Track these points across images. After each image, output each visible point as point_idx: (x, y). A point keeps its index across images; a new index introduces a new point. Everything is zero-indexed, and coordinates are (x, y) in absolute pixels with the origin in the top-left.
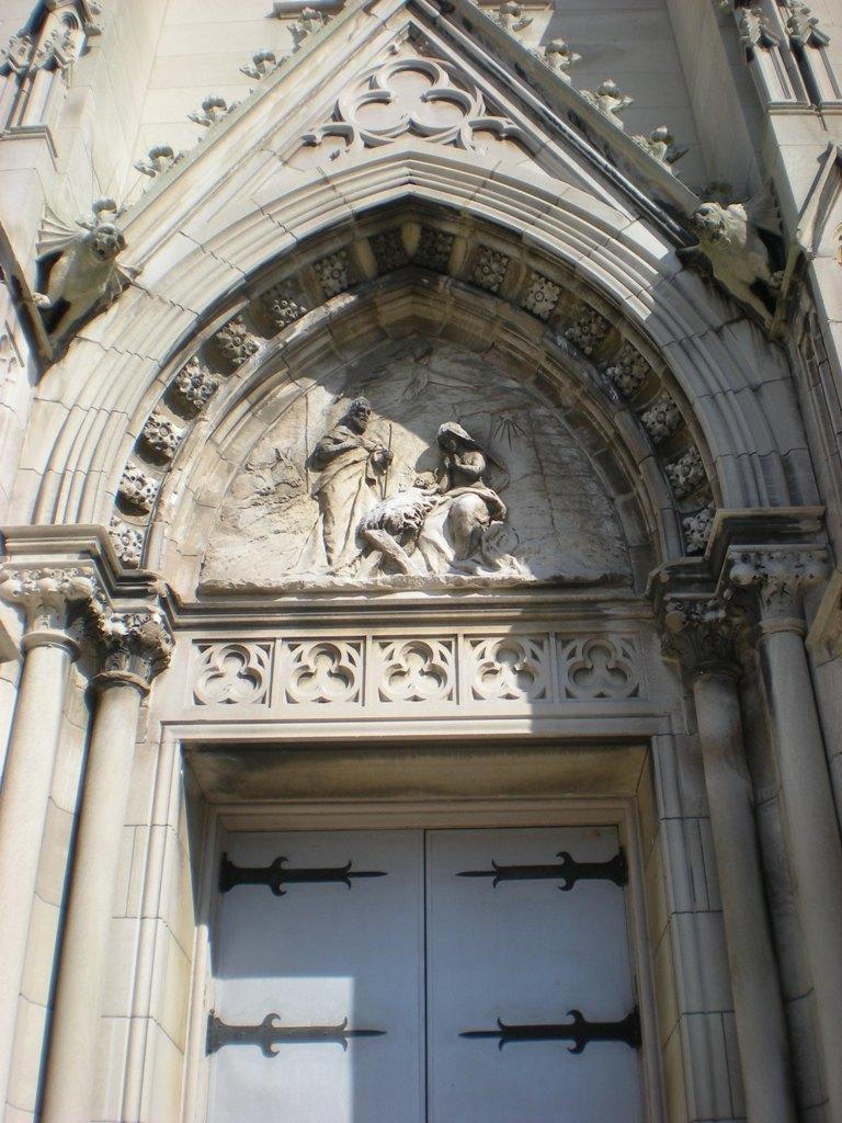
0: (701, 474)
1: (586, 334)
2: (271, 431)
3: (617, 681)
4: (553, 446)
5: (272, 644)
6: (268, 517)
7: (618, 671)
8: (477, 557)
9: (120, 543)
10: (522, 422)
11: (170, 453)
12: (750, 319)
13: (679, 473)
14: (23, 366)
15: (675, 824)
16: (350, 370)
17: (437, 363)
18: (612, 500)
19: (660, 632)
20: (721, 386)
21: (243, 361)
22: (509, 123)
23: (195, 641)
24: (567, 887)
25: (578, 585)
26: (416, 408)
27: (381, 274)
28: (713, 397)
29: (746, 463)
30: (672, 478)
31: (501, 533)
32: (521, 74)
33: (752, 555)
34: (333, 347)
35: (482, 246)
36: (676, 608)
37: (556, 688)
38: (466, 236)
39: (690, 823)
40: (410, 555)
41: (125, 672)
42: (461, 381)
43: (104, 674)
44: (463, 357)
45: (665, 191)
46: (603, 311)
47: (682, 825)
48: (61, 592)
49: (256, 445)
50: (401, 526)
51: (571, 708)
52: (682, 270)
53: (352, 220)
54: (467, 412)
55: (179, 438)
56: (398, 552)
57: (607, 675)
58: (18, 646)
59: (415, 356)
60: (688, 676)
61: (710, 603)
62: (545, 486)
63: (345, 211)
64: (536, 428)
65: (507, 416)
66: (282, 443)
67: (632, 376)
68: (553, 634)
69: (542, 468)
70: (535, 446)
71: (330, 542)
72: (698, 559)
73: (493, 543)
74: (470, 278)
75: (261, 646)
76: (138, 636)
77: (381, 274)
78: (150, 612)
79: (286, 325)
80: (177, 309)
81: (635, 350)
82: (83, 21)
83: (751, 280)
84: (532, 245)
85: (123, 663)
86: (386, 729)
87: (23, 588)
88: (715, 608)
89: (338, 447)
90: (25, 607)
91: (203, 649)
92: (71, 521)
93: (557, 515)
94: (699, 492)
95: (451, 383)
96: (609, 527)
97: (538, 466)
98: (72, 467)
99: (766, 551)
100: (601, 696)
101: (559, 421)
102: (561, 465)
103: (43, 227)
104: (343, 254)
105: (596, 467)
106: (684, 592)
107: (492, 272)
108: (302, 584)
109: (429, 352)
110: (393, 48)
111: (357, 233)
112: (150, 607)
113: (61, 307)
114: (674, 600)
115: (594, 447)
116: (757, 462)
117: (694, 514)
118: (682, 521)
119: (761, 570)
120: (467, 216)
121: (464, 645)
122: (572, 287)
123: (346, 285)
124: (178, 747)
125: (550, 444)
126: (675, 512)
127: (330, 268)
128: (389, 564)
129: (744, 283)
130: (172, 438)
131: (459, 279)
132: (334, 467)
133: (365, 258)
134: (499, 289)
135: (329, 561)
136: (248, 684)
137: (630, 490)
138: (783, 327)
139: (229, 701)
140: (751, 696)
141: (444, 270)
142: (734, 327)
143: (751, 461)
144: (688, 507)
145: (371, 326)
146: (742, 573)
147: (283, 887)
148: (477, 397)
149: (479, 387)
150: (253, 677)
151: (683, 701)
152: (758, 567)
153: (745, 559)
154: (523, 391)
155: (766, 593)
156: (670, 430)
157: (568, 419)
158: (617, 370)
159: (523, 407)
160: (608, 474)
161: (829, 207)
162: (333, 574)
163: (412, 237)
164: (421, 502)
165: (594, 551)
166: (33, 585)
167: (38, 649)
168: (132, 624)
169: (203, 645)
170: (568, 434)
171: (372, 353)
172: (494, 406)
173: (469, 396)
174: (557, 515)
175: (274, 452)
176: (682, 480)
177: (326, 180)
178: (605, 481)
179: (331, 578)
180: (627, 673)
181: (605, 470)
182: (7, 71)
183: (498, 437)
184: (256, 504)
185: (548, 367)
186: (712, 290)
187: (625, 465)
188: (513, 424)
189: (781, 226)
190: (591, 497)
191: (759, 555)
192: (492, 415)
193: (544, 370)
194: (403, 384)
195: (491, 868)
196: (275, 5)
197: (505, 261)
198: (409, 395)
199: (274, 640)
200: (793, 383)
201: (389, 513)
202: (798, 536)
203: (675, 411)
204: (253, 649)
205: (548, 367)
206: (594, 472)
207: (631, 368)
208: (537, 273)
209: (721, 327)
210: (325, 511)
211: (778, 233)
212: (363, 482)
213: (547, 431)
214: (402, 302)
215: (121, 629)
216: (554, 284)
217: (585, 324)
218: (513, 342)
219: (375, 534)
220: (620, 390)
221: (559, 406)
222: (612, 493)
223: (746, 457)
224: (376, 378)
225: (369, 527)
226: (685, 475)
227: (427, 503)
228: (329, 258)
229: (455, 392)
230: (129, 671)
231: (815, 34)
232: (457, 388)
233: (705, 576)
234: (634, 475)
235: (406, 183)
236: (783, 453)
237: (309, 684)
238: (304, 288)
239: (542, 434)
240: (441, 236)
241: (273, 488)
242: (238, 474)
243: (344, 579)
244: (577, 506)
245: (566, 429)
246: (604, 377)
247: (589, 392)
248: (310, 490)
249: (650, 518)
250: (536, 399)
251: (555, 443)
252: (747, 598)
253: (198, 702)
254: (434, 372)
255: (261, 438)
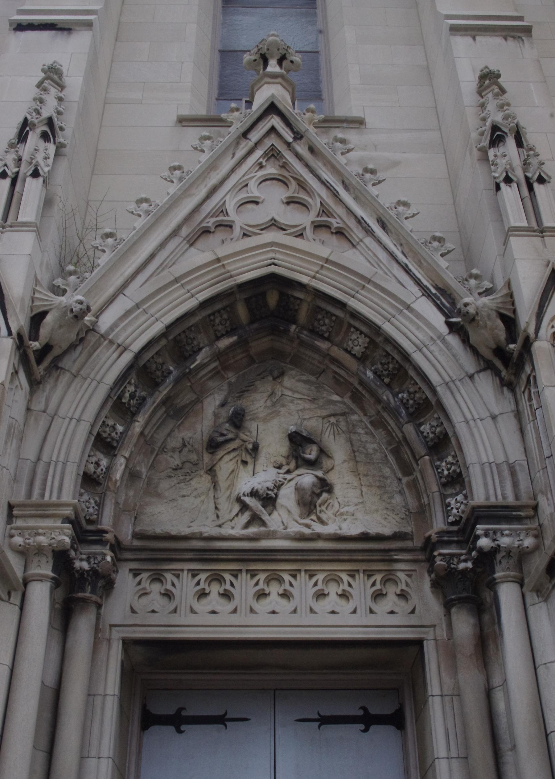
0: (458, 471)
1: (386, 370)
2: (179, 425)
3: (402, 603)
4: (362, 442)
5: (181, 573)
6: (177, 485)
7: (403, 595)
8: (314, 517)
9: (84, 507)
10: (343, 424)
11: (115, 444)
12: (491, 369)
13: (444, 468)
14: (22, 389)
15: (437, 700)
16: (230, 384)
17: (287, 381)
18: (400, 480)
19: (430, 572)
20: (476, 411)
21: (162, 380)
22: (338, 223)
23: (131, 570)
24: (366, 730)
25: (379, 538)
26: (272, 413)
27: (252, 322)
28: (467, 423)
29: (487, 470)
30: (439, 471)
31: (329, 501)
32: (346, 187)
33: (491, 532)
34: (220, 368)
35: (319, 307)
36: (441, 560)
37: (363, 606)
38: (309, 300)
39: (447, 699)
40: (270, 515)
41: (88, 594)
42: (304, 395)
43: (74, 595)
44: (304, 378)
45: (442, 279)
46: (397, 357)
47: (442, 699)
48: (50, 545)
49: (169, 435)
50: (265, 495)
51: (371, 620)
52: (449, 333)
53: (235, 289)
54: (307, 417)
55: (121, 433)
56: (263, 513)
57: (395, 598)
58: (21, 580)
59: (273, 377)
60: (448, 606)
61: (463, 557)
62: (357, 469)
63: (230, 283)
64: (351, 430)
65: (332, 420)
66: (186, 434)
67: (415, 401)
68: (362, 571)
69: (355, 456)
70: (351, 441)
71: (218, 504)
72: (455, 528)
73: (323, 508)
74: (311, 327)
75: (173, 574)
76: (97, 571)
77: (252, 322)
78: (104, 555)
79: (190, 355)
80: (121, 348)
81: (417, 384)
82: (54, 137)
83: (494, 346)
84: (351, 310)
85: (87, 588)
86: (255, 633)
87: (25, 543)
88: (465, 561)
89: (221, 439)
90: (23, 553)
91: (136, 575)
92: (54, 499)
93: (364, 489)
94: (457, 480)
95: (297, 395)
96: (398, 499)
97: (352, 455)
98: (54, 458)
99: (500, 529)
100: (392, 612)
101: (366, 425)
102: (367, 455)
103: (34, 294)
104: (228, 309)
105: (391, 458)
106: (446, 550)
107: (324, 324)
108: (201, 533)
109: (282, 374)
110: (260, 164)
111: (238, 296)
112: (104, 551)
113: (47, 348)
114: (440, 554)
115: (389, 443)
116: (494, 469)
117: (452, 496)
118: (445, 500)
119: (496, 542)
120: (310, 289)
121: (303, 576)
122: (379, 340)
123: (229, 329)
124: (121, 642)
125: (360, 441)
126: (441, 494)
127: (219, 318)
128: (255, 519)
129: (491, 348)
130: (116, 433)
131: (303, 328)
132: (221, 453)
133: (242, 312)
134: (329, 336)
135: (218, 517)
136: (166, 599)
137: (412, 474)
138: (513, 378)
139: (153, 611)
140: (486, 618)
141: (294, 321)
142: (481, 375)
143: (491, 468)
144: (449, 491)
145: (244, 355)
146: (484, 542)
147: (183, 728)
148: (313, 406)
149: (314, 399)
150: (168, 595)
151: (443, 618)
152: (494, 540)
153: (486, 535)
154: (343, 403)
155: (499, 557)
156: (439, 438)
157: (371, 423)
158: (405, 395)
159: (343, 414)
160: (397, 462)
161: (546, 305)
162: (220, 526)
163: (272, 299)
164: (278, 479)
165: (388, 515)
166: (31, 541)
167: (34, 583)
168: (93, 562)
169: (136, 573)
170: (372, 433)
171: (245, 372)
172: (324, 413)
173: (307, 406)
174: (364, 489)
175: (181, 440)
176: (446, 472)
177: (218, 260)
178: (395, 467)
179: (218, 529)
180: (408, 597)
181: (396, 459)
182: (4, 175)
183: (327, 434)
184: (170, 477)
185: (360, 389)
186: (468, 349)
187: (408, 456)
188: (337, 425)
189: (514, 311)
190: (386, 478)
191: (495, 532)
192: (323, 418)
193: (356, 389)
194: (266, 394)
195: (317, 717)
196: (178, 116)
197: (334, 318)
198: (269, 403)
199: (182, 570)
200: (518, 415)
201: (257, 487)
202: (519, 519)
203: (442, 427)
204: (287, 577)
205: (360, 389)
206: (388, 460)
207: (414, 395)
208: (355, 327)
209: (474, 374)
210: (215, 485)
211: (513, 316)
212: (239, 462)
213: (358, 431)
214: (265, 339)
215: (85, 565)
216: (366, 336)
217: (385, 364)
218: (337, 370)
219: (248, 500)
220: (407, 409)
221: (365, 415)
222: (400, 475)
223: (487, 464)
224: (248, 390)
225: (244, 495)
226: (448, 470)
227: (280, 479)
228: (219, 311)
229: (300, 402)
230: (90, 593)
231: (542, 174)
232: (301, 399)
233: (460, 538)
234: (415, 465)
235: (270, 265)
236: (511, 462)
237: (204, 601)
238: (202, 330)
239: (355, 433)
240: (292, 299)
241: (180, 465)
242: (157, 455)
243: (227, 531)
244: (378, 484)
245: (371, 431)
246: (396, 399)
247: (386, 408)
248: (205, 467)
249: (425, 496)
250: (352, 409)
251: (364, 439)
252: (487, 559)
253: (133, 611)
254: (286, 388)
255: (172, 431)
